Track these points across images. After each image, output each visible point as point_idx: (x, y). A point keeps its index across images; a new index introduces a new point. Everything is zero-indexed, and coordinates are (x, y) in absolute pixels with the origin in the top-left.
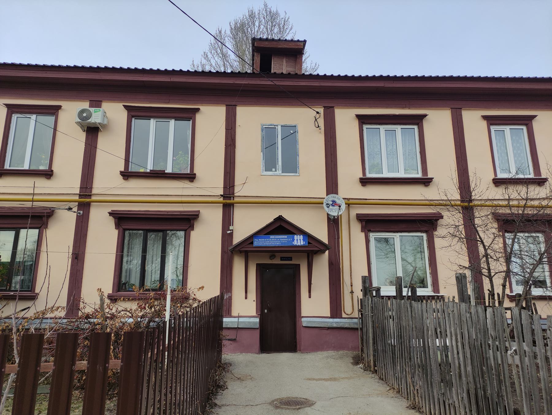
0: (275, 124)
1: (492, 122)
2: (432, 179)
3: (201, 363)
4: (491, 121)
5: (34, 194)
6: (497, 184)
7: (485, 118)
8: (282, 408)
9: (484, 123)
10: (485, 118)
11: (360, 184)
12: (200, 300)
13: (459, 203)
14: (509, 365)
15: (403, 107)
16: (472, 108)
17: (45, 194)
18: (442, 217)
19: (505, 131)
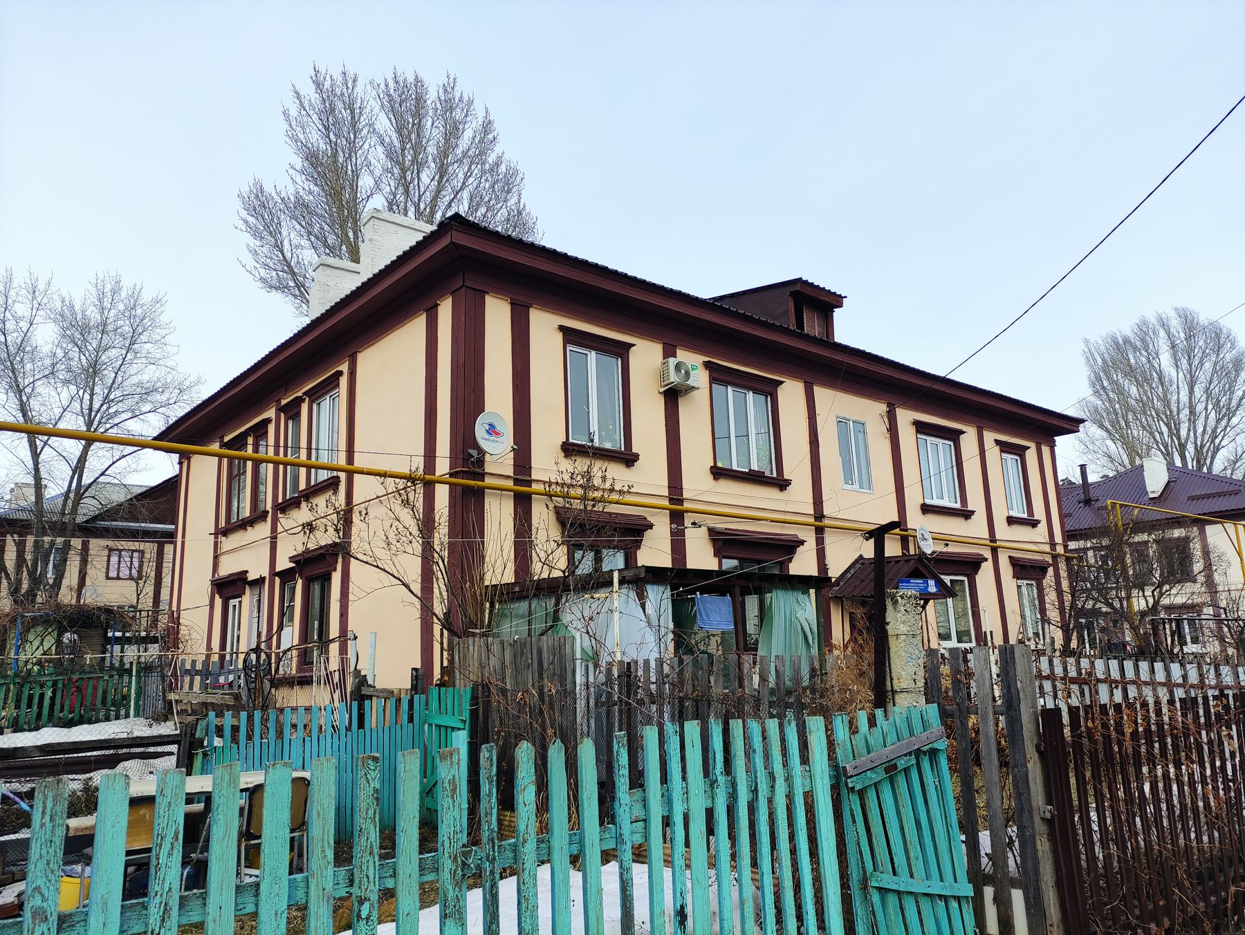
0: (848, 417)
1: (1006, 449)
2: (973, 512)
3: (763, 829)
4: (570, 336)
5: (317, 449)
6: (716, 476)
7: (562, 328)
8: (807, 924)
9: (559, 337)
10: (562, 328)
11: (711, 477)
12: (118, 721)
13: (510, 483)
14: (668, 862)
15: (943, 417)
16: (499, 294)
17: (501, 475)
18: (651, 526)
19: (589, 355)
